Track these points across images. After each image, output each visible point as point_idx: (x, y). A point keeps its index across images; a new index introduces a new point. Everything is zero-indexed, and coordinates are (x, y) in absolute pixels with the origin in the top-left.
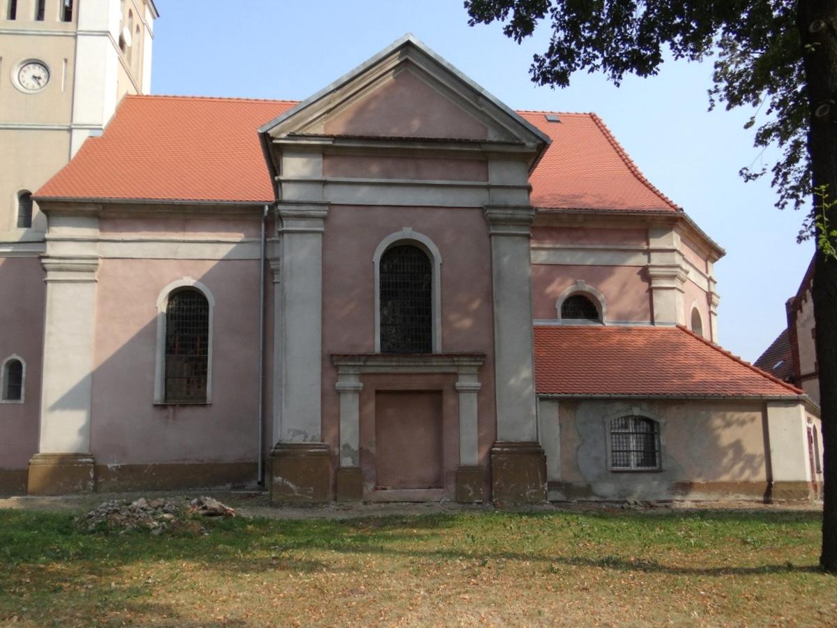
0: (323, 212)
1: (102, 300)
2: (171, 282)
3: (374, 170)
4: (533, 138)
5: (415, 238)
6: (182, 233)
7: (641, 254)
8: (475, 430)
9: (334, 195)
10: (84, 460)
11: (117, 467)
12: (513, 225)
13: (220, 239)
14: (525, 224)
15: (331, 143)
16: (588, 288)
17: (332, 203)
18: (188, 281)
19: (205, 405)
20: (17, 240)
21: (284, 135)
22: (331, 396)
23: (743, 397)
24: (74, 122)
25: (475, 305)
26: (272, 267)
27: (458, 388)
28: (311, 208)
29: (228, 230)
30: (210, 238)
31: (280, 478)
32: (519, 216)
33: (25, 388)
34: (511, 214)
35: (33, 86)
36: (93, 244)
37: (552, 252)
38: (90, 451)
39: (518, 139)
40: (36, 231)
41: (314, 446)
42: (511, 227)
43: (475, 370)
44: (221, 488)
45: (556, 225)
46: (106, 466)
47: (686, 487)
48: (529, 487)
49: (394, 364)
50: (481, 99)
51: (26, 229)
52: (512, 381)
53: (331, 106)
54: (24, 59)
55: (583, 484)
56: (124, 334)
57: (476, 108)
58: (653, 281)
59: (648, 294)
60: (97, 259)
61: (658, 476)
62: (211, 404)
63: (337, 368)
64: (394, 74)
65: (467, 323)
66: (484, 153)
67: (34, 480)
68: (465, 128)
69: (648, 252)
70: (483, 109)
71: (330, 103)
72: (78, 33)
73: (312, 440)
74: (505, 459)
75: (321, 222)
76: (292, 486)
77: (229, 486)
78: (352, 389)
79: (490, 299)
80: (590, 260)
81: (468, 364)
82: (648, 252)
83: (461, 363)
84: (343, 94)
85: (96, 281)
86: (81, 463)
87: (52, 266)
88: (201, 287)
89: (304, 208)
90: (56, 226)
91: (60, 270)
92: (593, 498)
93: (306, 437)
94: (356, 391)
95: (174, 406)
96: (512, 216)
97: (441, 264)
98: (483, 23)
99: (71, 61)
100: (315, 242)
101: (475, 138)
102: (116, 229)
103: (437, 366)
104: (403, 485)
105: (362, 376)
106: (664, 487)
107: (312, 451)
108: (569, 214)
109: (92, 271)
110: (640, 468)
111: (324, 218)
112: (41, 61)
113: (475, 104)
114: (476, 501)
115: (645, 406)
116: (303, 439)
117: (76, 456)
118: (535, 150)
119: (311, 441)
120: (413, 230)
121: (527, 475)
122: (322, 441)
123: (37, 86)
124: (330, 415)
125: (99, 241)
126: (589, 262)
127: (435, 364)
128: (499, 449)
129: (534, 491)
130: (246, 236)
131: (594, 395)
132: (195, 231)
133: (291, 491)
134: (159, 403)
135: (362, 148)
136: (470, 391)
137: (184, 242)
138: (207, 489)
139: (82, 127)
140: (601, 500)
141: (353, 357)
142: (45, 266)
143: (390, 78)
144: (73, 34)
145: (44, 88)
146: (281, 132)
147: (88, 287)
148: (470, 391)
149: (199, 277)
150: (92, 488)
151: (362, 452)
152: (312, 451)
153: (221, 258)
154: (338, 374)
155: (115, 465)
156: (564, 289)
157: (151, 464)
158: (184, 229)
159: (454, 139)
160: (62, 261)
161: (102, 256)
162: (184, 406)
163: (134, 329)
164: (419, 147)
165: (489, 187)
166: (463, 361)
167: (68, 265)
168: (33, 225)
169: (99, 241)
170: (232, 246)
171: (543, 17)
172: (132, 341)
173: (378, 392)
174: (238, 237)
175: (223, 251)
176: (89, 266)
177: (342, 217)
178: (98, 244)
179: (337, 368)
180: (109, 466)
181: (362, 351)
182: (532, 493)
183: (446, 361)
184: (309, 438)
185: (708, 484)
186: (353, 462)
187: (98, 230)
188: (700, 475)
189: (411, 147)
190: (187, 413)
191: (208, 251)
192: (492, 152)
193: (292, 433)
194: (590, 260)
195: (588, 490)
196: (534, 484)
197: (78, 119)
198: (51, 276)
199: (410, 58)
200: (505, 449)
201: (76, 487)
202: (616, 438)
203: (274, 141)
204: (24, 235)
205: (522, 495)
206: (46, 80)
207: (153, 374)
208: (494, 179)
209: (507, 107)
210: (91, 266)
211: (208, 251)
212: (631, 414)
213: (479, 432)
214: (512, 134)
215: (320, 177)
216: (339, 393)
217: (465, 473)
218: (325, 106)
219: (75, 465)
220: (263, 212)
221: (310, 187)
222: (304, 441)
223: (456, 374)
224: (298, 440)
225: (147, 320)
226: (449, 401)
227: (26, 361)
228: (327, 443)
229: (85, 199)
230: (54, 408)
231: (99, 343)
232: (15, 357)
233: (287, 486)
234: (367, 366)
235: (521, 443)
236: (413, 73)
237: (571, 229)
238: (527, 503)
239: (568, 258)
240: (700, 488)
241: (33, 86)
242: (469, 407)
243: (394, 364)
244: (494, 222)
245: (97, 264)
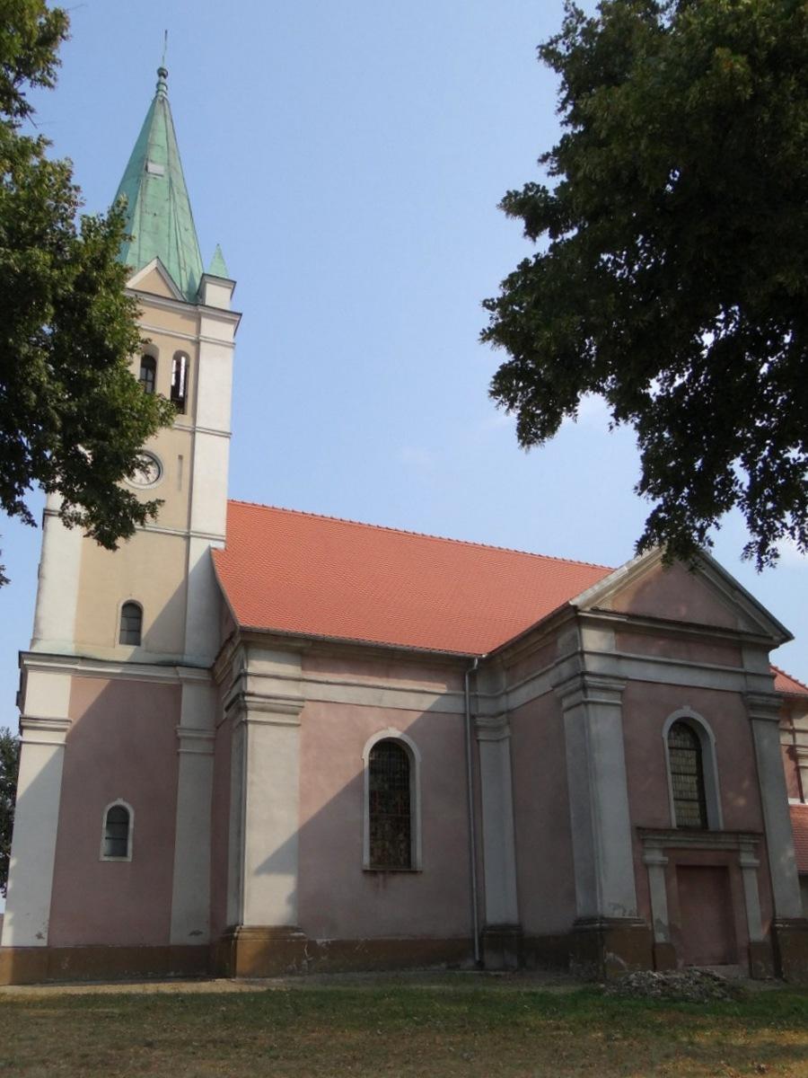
1: (306, 747)
2: (377, 732)
3: (654, 650)
4: (780, 633)
6: (385, 679)
7: (787, 733)
10: (296, 934)
11: (327, 943)
13: (426, 689)
15: (625, 620)
17: (631, 677)
18: (394, 733)
19: (415, 872)
20: (125, 659)
21: (588, 609)
22: (642, 869)
24: (192, 529)
26: (479, 723)
28: (612, 681)
29: (430, 680)
30: (370, 683)
31: (611, 954)
33: (134, 842)
35: (141, 480)
36: (297, 683)
39: (766, 632)
40: (146, 651)
41: (635, 921)
43: (751, 848)
44: (436, 967)
46: (315, 942)
50: (737, 593)
51: (135, 647)
56: (329, 788)
58: (800, 760)
59: (795, 773)
60: (303, 700)
62: (421, 872)
63: (643, 841)
67: (246, 952)
68: (721, 617)
69: (793, 732)
70: (736, 601)
72: (197, 429)
73: (630, 915)
75: (619, 695)
76: (622, 962)
77: (444, 965)
81: (747, 841)
82: (793, 732)
83: (745, 841)
86: (294, 938)
87: (254, 705)
88: (407, 739)
89: (607, 681)
90: (257, 659)
91: (263, 710)
93: (625, 911)
94: (663, 866)
95: (383, 872)
99: (187, 459)
100: (614, 714)
102: (317, 668)
105: (666, 851)
109: (297, 714)
112: (152, 454)
113: (730, 596)
117: (285, 929)
123: (145, 481)
124: (644, 893)
125: (304, 680)
128: (781, 926)
130: (449, 688)
132: (399, 678)
134: (368, 869)
135: (647, 627)
137: (390, 689)
138: (422, 968)
139: (203, 536)
141: (656, 831)
142: (248, 704)
144: (190, 429)
145: (155, 485)
147: (292, 732)
149: (405, 728)
151: (672, 929)
153: (425, 709)
155: (325, 940)
157: (362, 940)
158: (388, 676)
160: (267, 700)
162: (394, 872)
163: (340, 783)
164: (693, 631)
165: (746, 674)
167: (273, 705)
168: (143, 643)
170: (436, 698)
172: (339, 795)
173: (680, 868)
174: (442, 688)
175: (427, 702)
176: (293, 708)
178: (302, 684)
179: (643, 841)
180: (319, 941)
184: (627, 913)
186: (665, 938)
187: (299, 668)
189: (684, 630)
190: (397, 881)
191: (412, 701)
193: (612, 907)
197: (195, 527)
198: (252, 716)
200: (787, 926)
201: (290, 966)
203: (580, 614)
204: (133, 655)
206: (156, 476)
207: (362, 835)
210: (297, 709)
211: (412, 701)
214: (762, 628)
215: (614, 652)
217: (753, 949)
219: (288, 941)
220: (473, 666)
221: (608, 661)
224: (618, 914)
225: (353, 774)
226: (735, 877)
227: (134, 808)
228: (641, 917)
230: (259, 871)
231: (304, 798)
232: (120, 802)
233: (618, 962)
235: (795, 919)
241: (141, 480)
242: (751, 881)
244: (753, 707)
245: (302, 707)
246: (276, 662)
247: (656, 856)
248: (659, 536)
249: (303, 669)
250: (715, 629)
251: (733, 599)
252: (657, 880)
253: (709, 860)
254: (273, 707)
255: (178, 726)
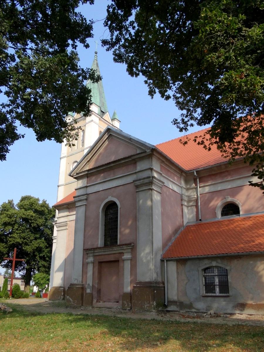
0: (85, 197)
3: (101, 178)
5: (113, 200)
8: (129, 277)
9: (90, 190)
12: (145, 186)
14: (149, 184)
15: (87, 172)
16: (230, 199)
21: (75, 174)
23: (261, 252)
25: (130, 223)
27: (123, 259)
28: (82, 197)
32: (145, 182)
34: (142, 182)
37: (212, 186)
38: (64, 286)
42: (144, 187)
43: (130, 250)
45: (213, 173)
47: (242, 306)
48: (146, 303)
49: (102, 251)
52: (142, 254)
53: (88, 160)
54: (72, 163)
55: (188, 303)
57: (130, 143)
60: (67, 222)
61: (228, 299)
63: (87, 254)
64: (108, 140)
65: (127, 231)
66: (134, 160)
70: (132, 143)
71: (87, 159)
74: (137, 289)
75: (85, 201)
76: (71, 300)
78: (90, 262)
79: (135, 219)
80: (228, 186)
81: (126, 248)
83: (124, 248)
84: (91, 154)
85: (67, 229)
92: (194, 310)
96: (143, 182)
97: (120, 208)
98: (36, 134)
101: (124, 157)
103: (116, 250)
104: (109, 301)
106: (231, 305)
107: (77, 286)
108: (217, 167)
109: (66, 226)
110: (220, 295)
111: (86, 199)
114: (128, 309)
115: (219, 261)
116: (77, 282)
117: (60, 287)
118: (151, 152)
119: (79, 282)
120: (112, 197)
121: (145, 297)
122: (82, 282)
124: (84, 272)
125: (68, 216)
126: (229, 187)
127: (115, 249)
129: (148, 305)
131: (208, 256)
133: (70, 302)
136: (128, 260)
140: (197, 311)
143: (107, 143)
146: (74, 174)
147: (65, 231)
148: (128, 260)
150: (62, 298)
152: (77, 286)
154: (88, 256)
156: (218, 203)
159: (122, 158)
160: (60, 224)
161: (69, 221)
164: (112, 165)
166: (124, 247)
169: (68, 216)
171: (169, 95)
173: (100, 263)
177: (91, 198)
181: (95, 247)
182: (147, 306)
183: (119, 248)
185: (257, 305)
188: (252, 299)
192: (137, 158)
193: (74, 279)
194: (228, 186)
195: (190, 306)
196: (148, 302)
199: (111, 134)
202: (225, 278)
205: (143, 307)
208: (139, 168)
209: (138, 139)
212: (211, 265)
213: (131, 277)
215: (86, 185)
216: (88, 263)
218: (86, 160)
222: (77, 282)
223: (123, 253)
229: (63, 204)
230: (56, 271)
233: (70, 300)
234: (95, 253)
236: (114, 138)
237: (221, 173)
238: (145, 311)
239: (219, 187)
240: (252, 306)
242: (127, 266)
243: (102, 251)
246: (63, 212)
247: (91, 259)
248: (233, 98)
249: (69, 212)
250: (119, 160)
251: (131, 142)
252: (90, 268)
253: (112, 258)
254: (61, 225)
255: (52, 236)
